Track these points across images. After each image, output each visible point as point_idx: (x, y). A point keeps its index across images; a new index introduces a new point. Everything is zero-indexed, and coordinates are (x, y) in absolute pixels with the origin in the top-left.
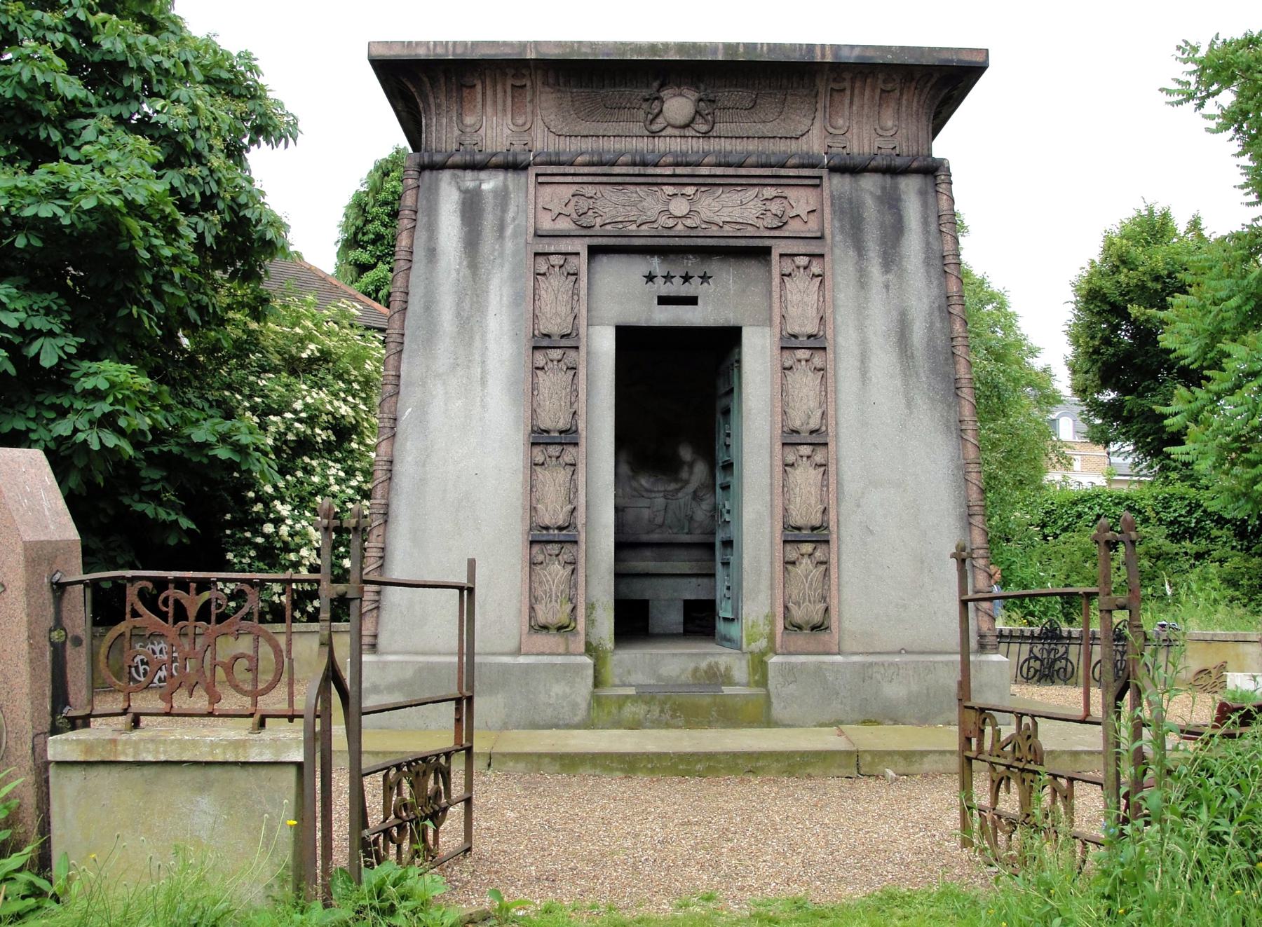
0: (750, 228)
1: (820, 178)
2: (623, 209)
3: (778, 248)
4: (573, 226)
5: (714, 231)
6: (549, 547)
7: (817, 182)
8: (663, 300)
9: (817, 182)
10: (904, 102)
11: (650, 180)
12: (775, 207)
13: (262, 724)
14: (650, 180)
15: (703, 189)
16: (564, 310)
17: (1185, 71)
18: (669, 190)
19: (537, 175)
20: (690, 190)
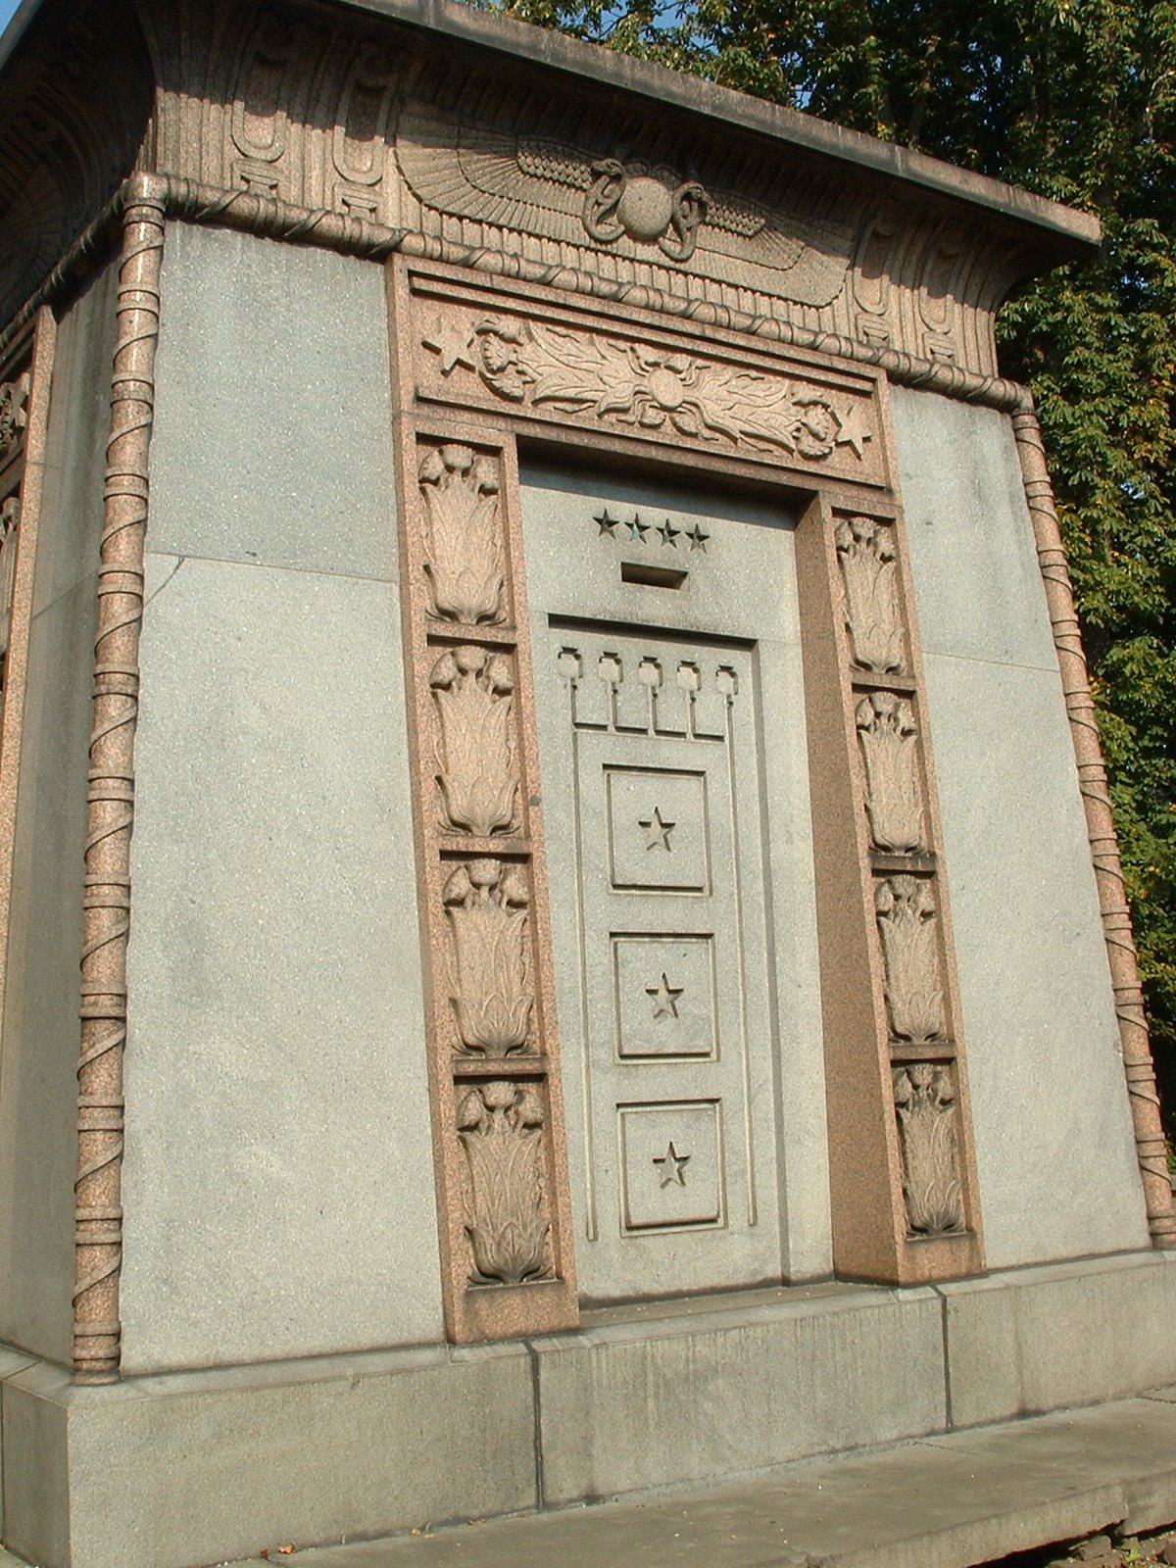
0: (778, 451)
1: (873, 381)
2: (585, 377)
3: (830, 498)
4: (483, 391)
5: (722, 446)
6: (621, 999)
7: (867, 386)
8: (634, 574)
9: (867, 386)
10: (928, 268)
11: (617, 328)
12: (816, 418)
13: (670, 826)
14: (617, 328)
15: (700, 362)
16: (482, 565)
17: (606, 534)
18: (648, 354)
19: (411, 274)
20: (681, 361)
